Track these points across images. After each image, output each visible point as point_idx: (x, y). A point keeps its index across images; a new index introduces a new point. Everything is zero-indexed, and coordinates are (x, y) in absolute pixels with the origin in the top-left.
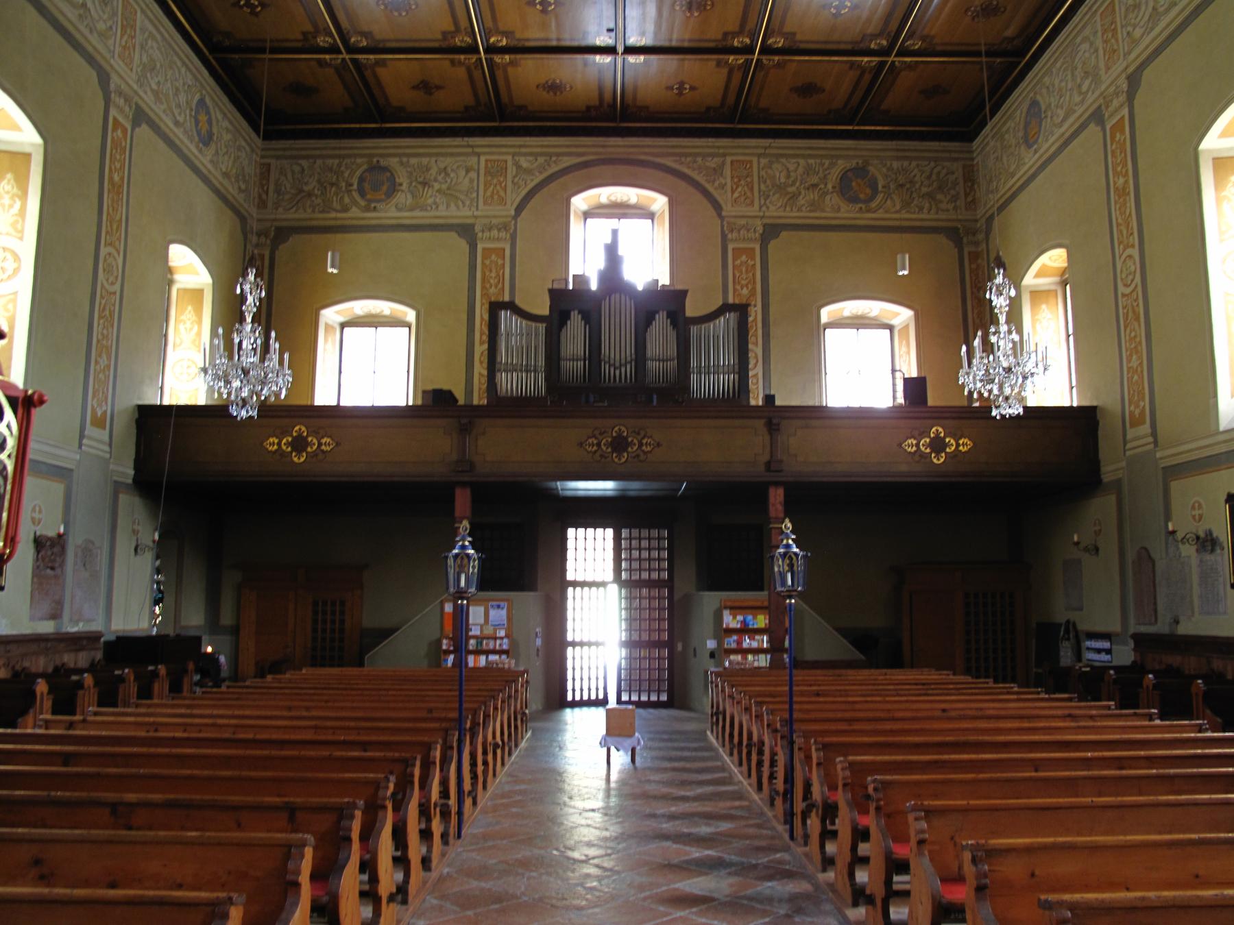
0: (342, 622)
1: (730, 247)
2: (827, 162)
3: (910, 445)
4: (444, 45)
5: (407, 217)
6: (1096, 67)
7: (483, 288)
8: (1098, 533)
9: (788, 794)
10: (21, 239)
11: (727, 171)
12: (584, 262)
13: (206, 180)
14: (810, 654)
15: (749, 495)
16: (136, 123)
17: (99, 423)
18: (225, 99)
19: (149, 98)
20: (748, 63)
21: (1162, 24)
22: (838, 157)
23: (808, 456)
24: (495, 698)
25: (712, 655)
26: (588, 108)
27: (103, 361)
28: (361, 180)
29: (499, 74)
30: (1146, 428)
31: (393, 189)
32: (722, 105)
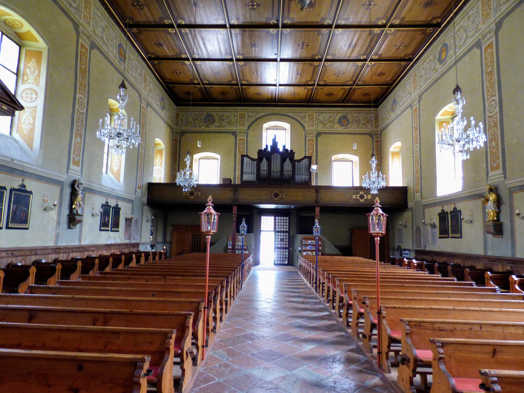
0: (200, 241)
1: (307, 139)
2: (335, 114)
3: (354, 197)
4: (229, 83)
5: (217, 129)
6: (411, 92)
7: (239, 149)
8: (407, 222)
9: (316, 283)
10: (38, 85)
11: (307, 117)
12: (266, 142)
13: (161, 117)
14: (327, 252)
15: (312, 209)
16: (147, 106)
17: (139, 188)
18: (168, 96)
19: (150, 99)
20: (313, 89)
21: (428, 83)
22: (339, 113)
23: (326, 199)
24: (234, 271)
25: (300, 252)
26: (268, 99)
27: (140, 172)
28: (205, 119)
29: (244, 91)
30: (419, 194)
31: (214, 121)
32: (306, 97)
